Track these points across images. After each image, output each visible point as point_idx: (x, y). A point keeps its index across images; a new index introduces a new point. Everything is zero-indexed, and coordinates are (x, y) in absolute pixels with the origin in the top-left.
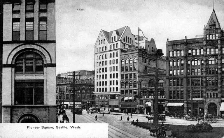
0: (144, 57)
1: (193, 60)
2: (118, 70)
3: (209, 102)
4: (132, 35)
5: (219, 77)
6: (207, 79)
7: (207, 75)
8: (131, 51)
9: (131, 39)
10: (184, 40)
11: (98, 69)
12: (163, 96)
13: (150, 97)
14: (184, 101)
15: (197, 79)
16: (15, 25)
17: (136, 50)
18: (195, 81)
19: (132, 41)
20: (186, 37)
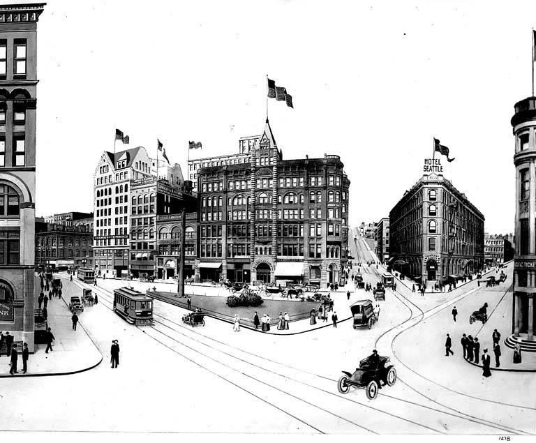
1: (235, 197)
13: (173, 253)
20: (307, 156)
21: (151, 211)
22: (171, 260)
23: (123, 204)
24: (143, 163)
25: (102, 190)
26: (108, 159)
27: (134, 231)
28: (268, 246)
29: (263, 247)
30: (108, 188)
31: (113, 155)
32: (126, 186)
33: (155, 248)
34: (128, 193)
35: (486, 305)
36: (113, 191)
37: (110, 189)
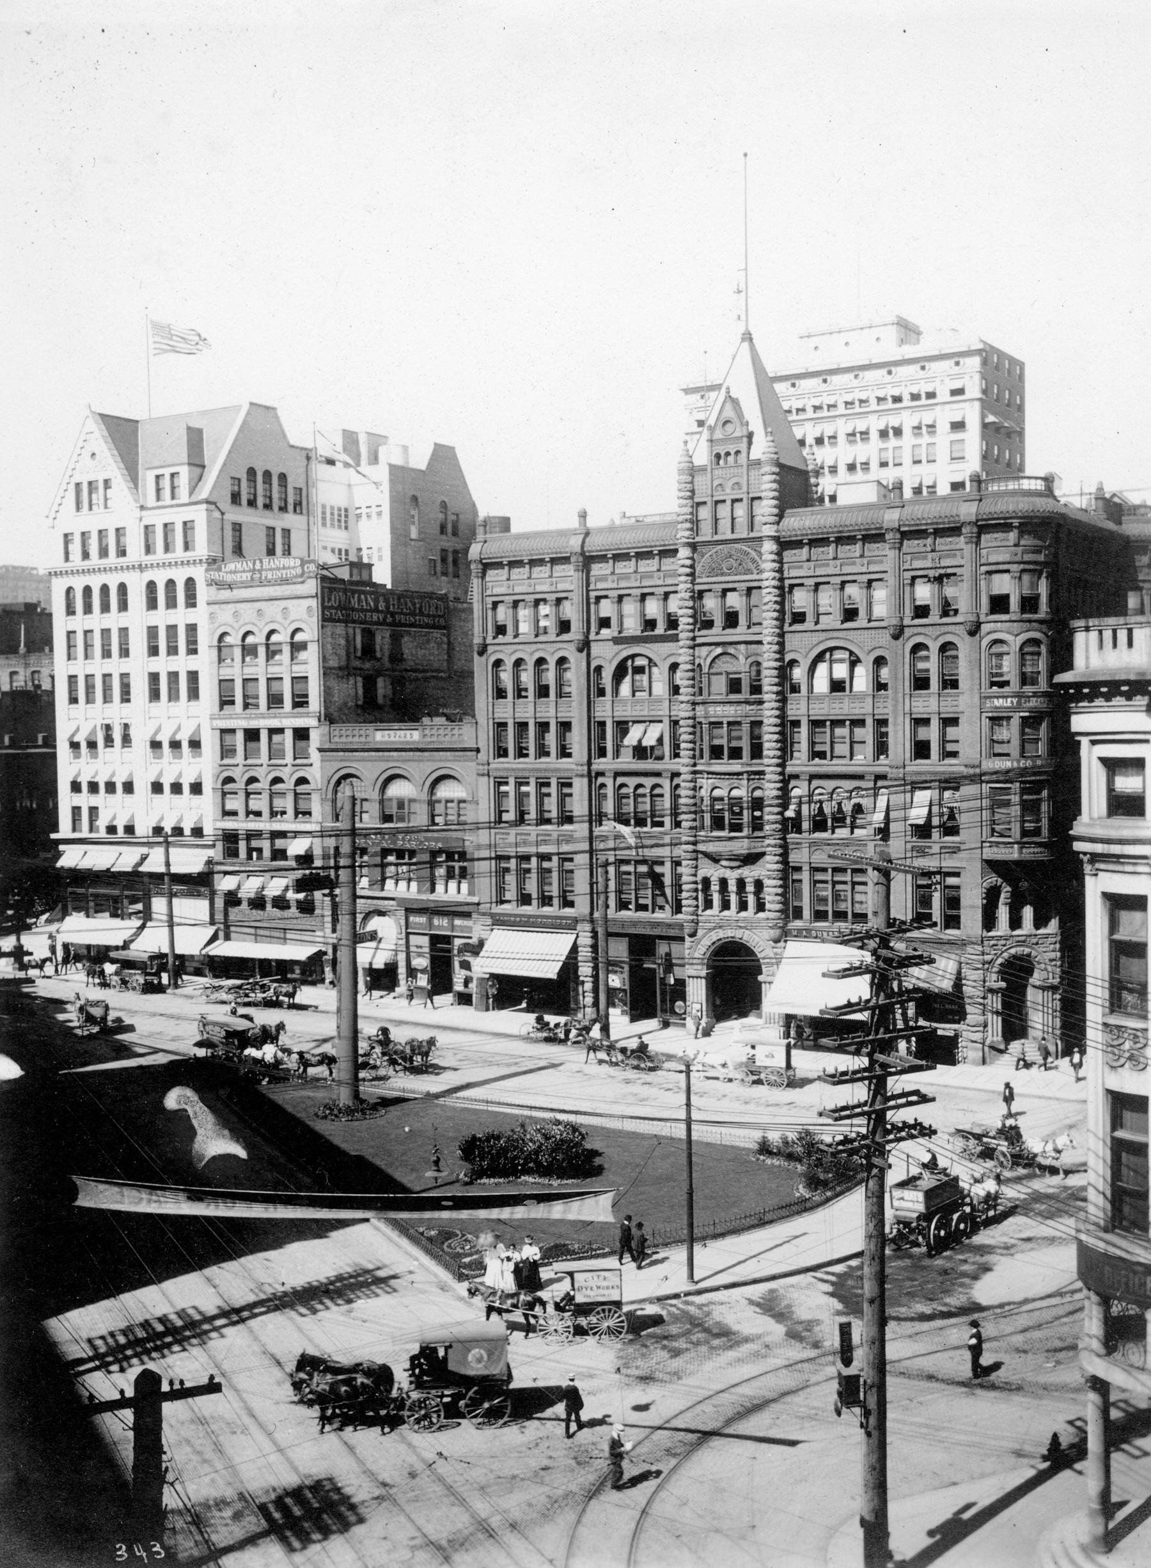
0: (355, 616)
1: (820, 658)
2: (75, 659)
3: (715, 936)
4: (292, 447)
5: (767, 777)
6: (703, 792)
7: (698, 768)
8: (270, 583)
9: (283, 477)
10: (562, 533)
11: (926, 722)
12: (464, 886)
13: (390, 884)
14: (576, 921)
15: (649, 782)
16: (839, 1078)
17: (302, 578)
18: (652, 796)
19: (290, 491)
20: (583, 516)
21: (300, 701)
22: (381, 913)
23: (182, 663)
24: (267, 475)
25: (105, 589)
26: (99, 442)
27: (229, 780)
28: (750, 873)
29: (732, 876)
30: (180, 576)
31: (132, 424)
32: (190, 583)
33: (318, 863)
34: (199, 615)
35: (824, 975)
36: (137, 597)
37: (123, 588)
